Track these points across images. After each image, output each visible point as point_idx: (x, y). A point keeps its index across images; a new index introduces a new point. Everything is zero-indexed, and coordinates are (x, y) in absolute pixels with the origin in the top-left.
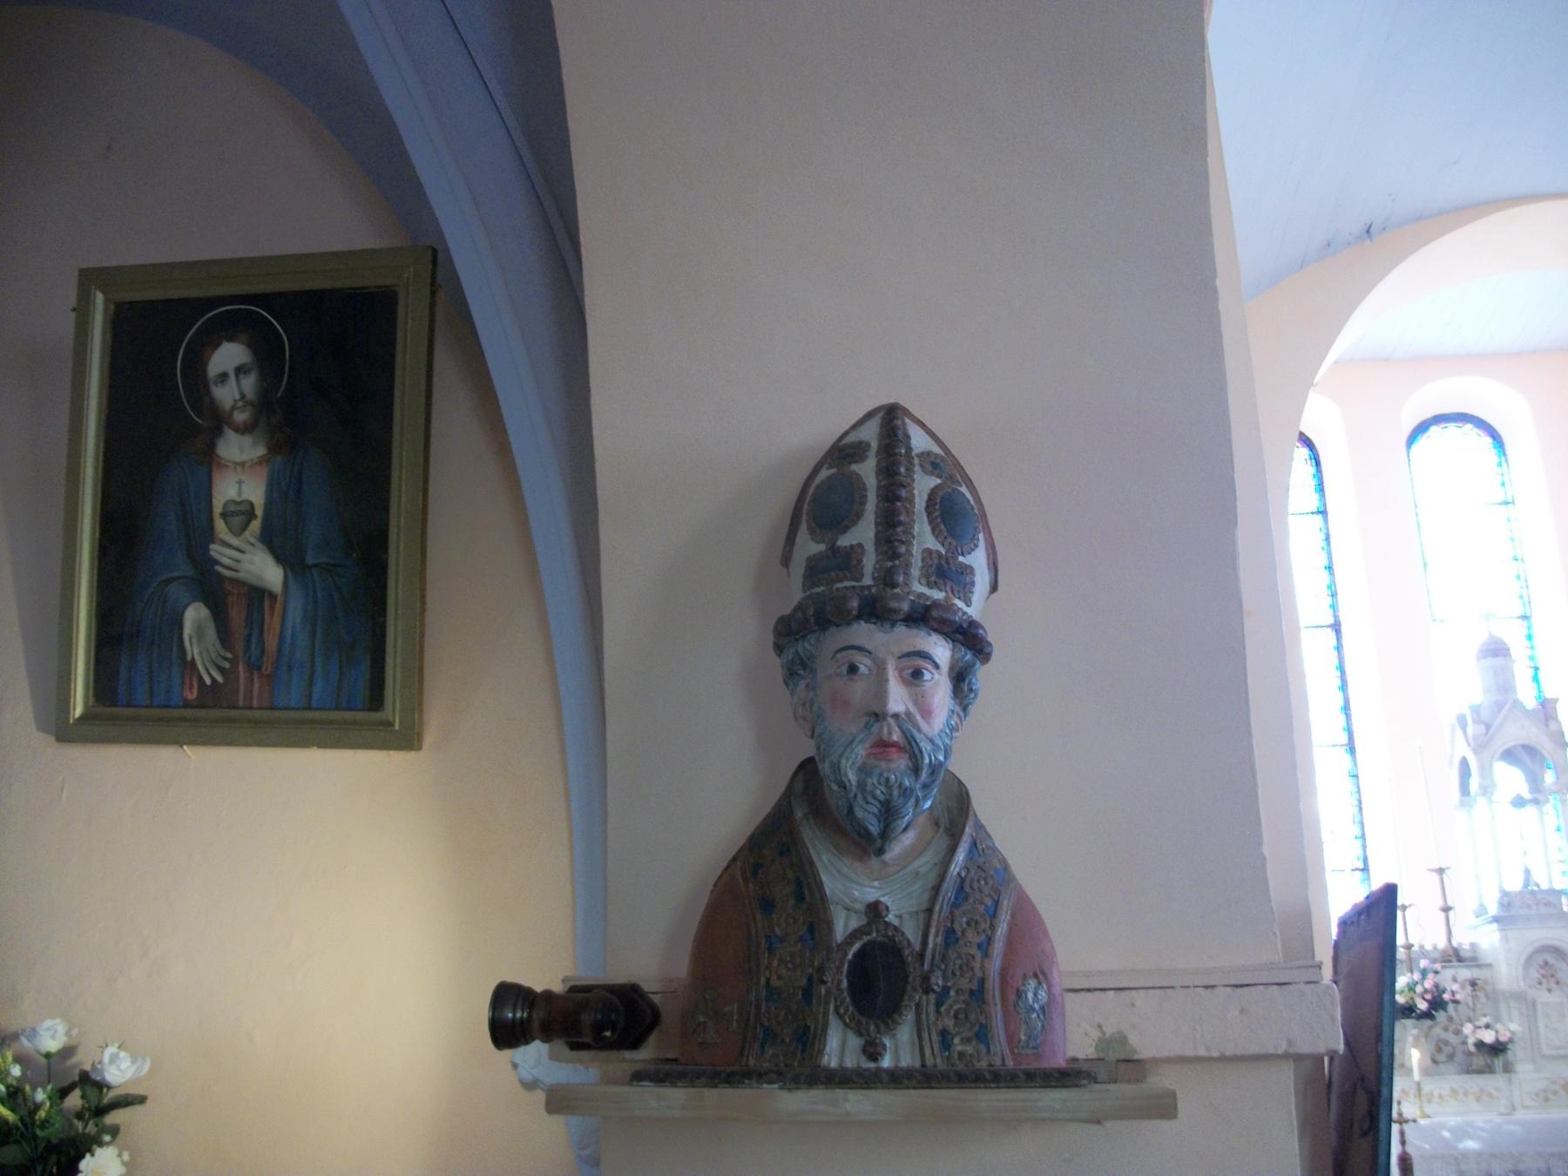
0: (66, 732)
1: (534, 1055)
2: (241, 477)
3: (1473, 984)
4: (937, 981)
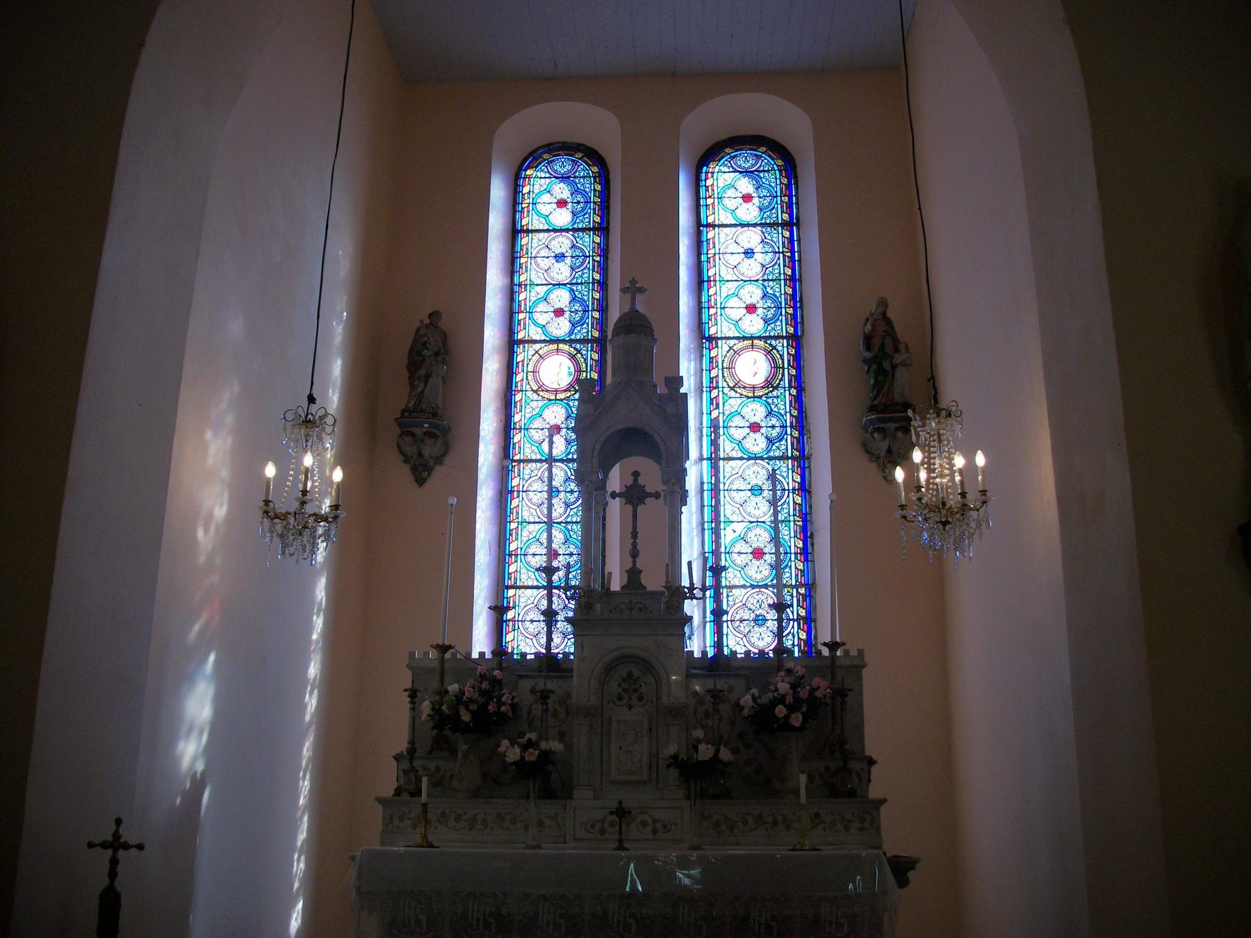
3: (545, 695)
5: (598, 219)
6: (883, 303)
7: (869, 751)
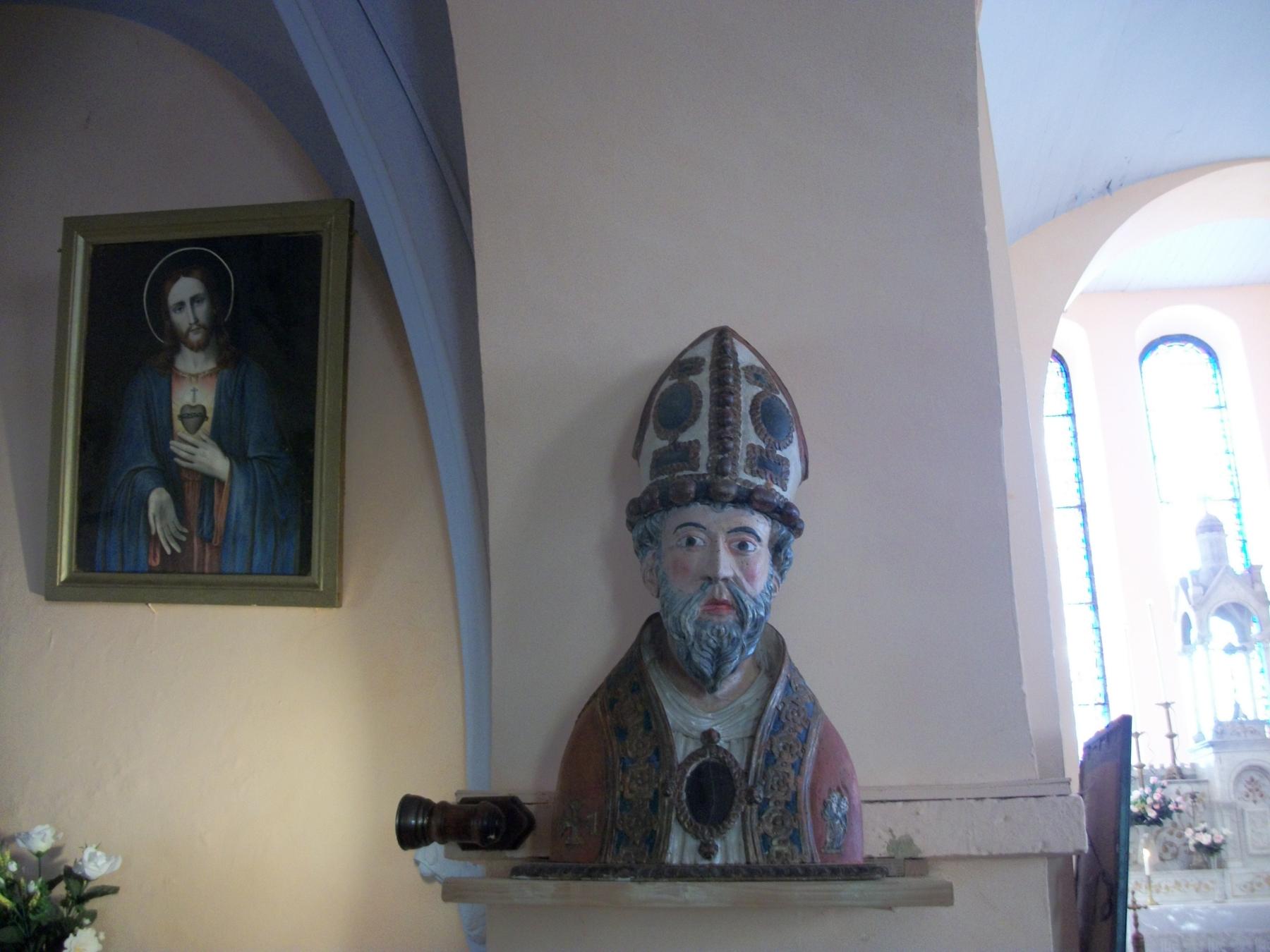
0: (53, 593)
1: (432, 854)
2: (195, 386)
3: (1193, 796)
4: (759, 794)
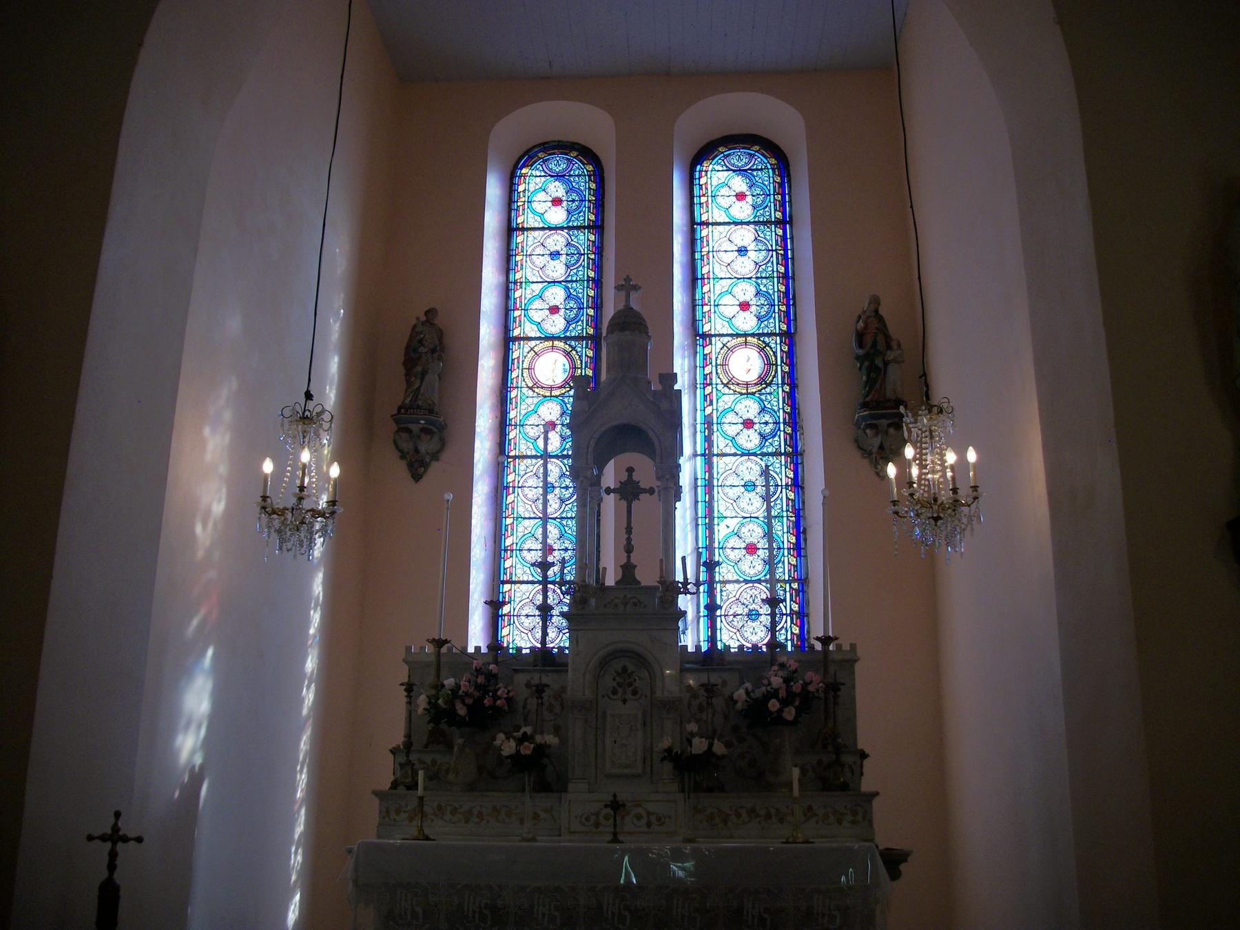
3: (540, 689)
5: (593, 217)
6: (876, 301)
7: (862, 744)
